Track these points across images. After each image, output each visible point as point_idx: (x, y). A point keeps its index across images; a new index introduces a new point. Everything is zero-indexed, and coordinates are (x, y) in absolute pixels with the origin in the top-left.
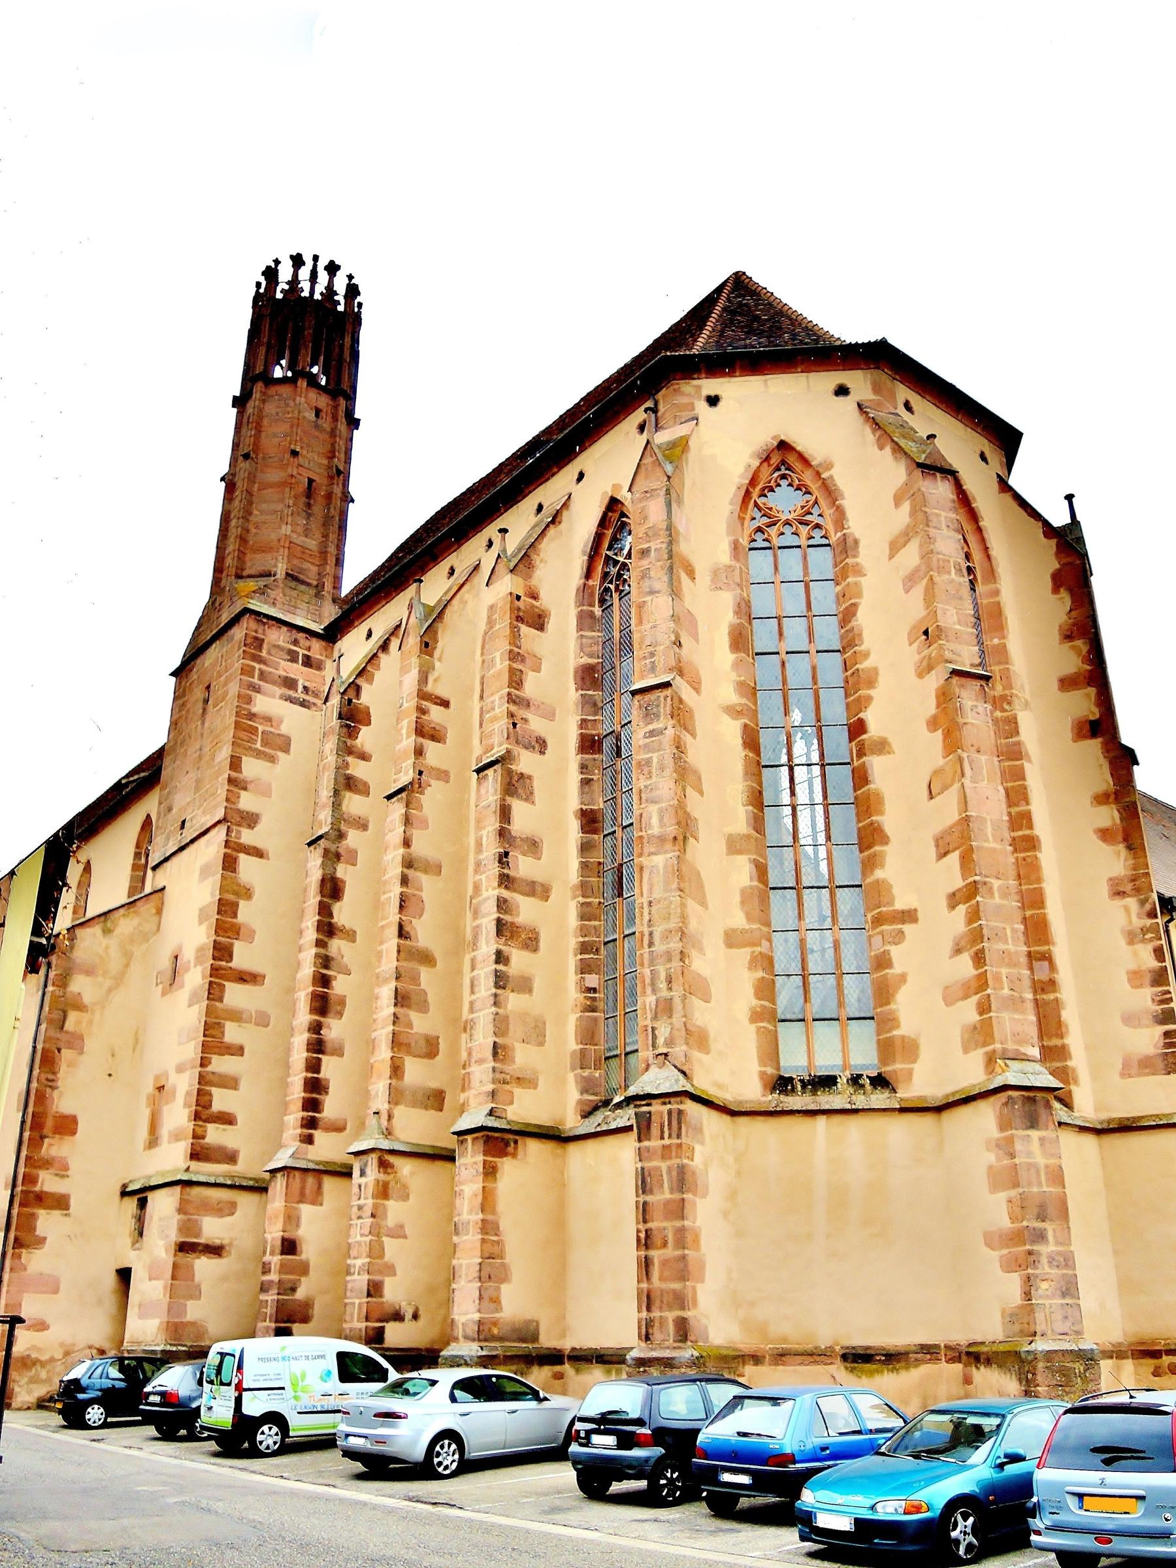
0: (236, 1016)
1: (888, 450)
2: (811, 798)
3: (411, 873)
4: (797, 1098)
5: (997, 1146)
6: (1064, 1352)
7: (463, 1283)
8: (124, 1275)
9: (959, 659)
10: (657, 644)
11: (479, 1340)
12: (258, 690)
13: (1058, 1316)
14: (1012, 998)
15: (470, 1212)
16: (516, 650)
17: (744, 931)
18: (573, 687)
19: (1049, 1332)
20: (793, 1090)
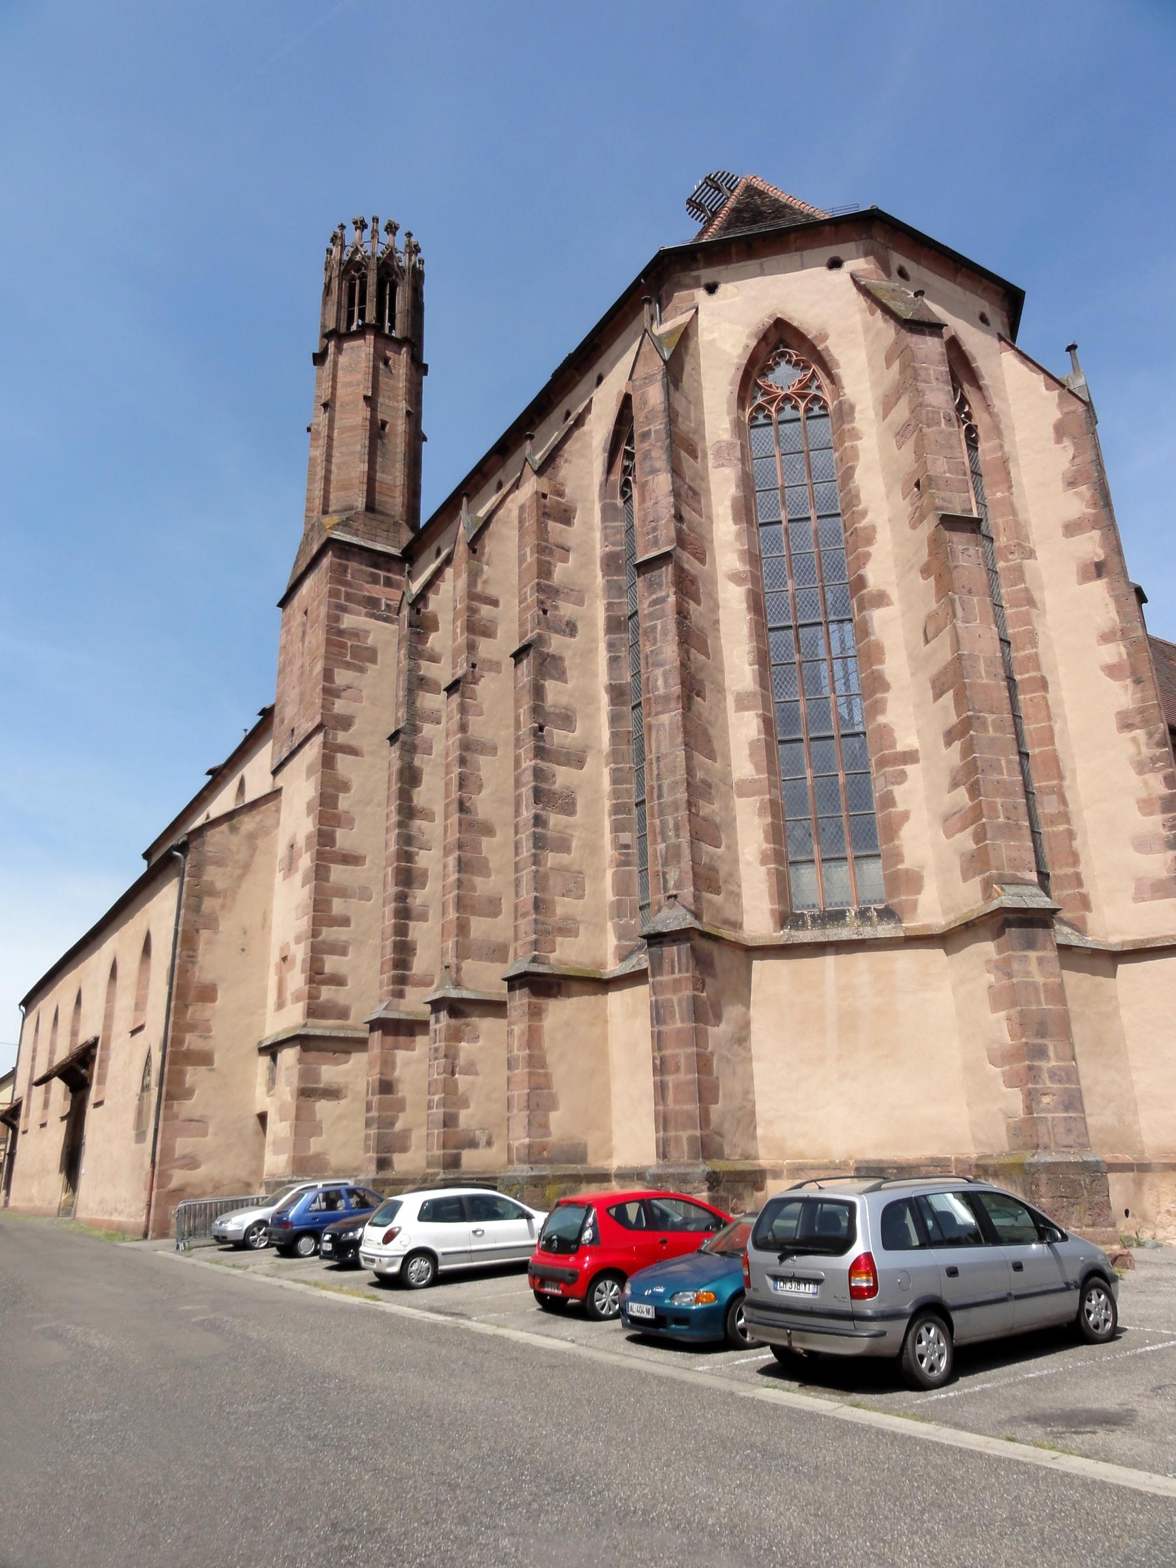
0: (343, 893)
1: (879, 313)
2: (845, 666)
3: (468, 755)
4: (808, 932)
5: (997, 967)
6: (1069, 1164)
7: (515, 1111)
9: (949, 505)
11: (530, 1163)
12: (344, 609)
13: (1061, 1129)
14: (1007, 826)
15: (519, 1050)
16: (544, 544)
17: (752, 781)
18: (599, 574)
19: (1052, 1145)
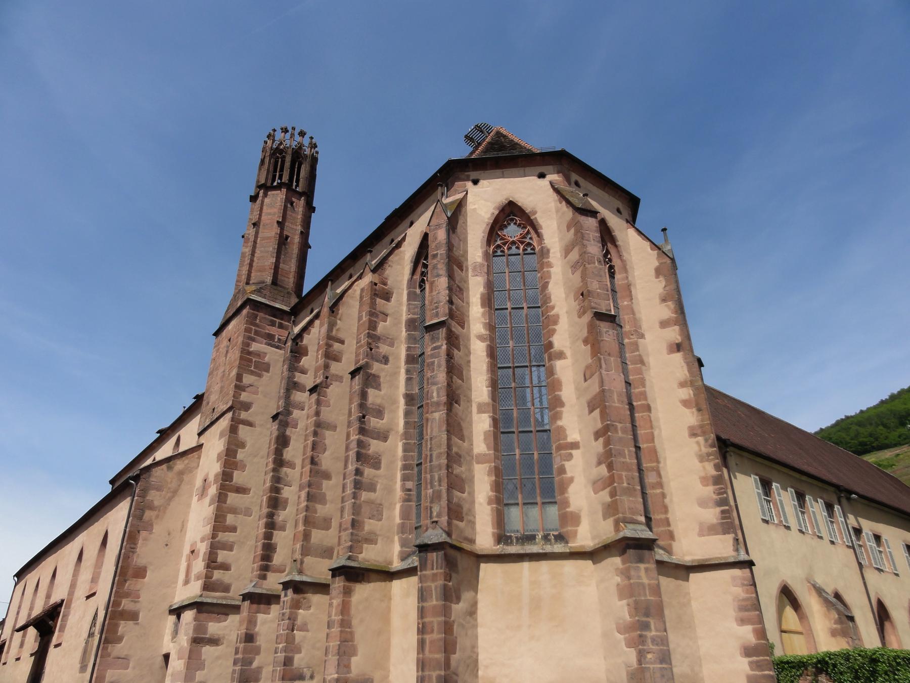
0: (234, 511)
1: (564, 203)
3: (319, 430)
8: (167, 657)
10: (440, 302)
14: (628, 488)
15: (335, 615)
18: (404, 330)
20: (512, 541)
